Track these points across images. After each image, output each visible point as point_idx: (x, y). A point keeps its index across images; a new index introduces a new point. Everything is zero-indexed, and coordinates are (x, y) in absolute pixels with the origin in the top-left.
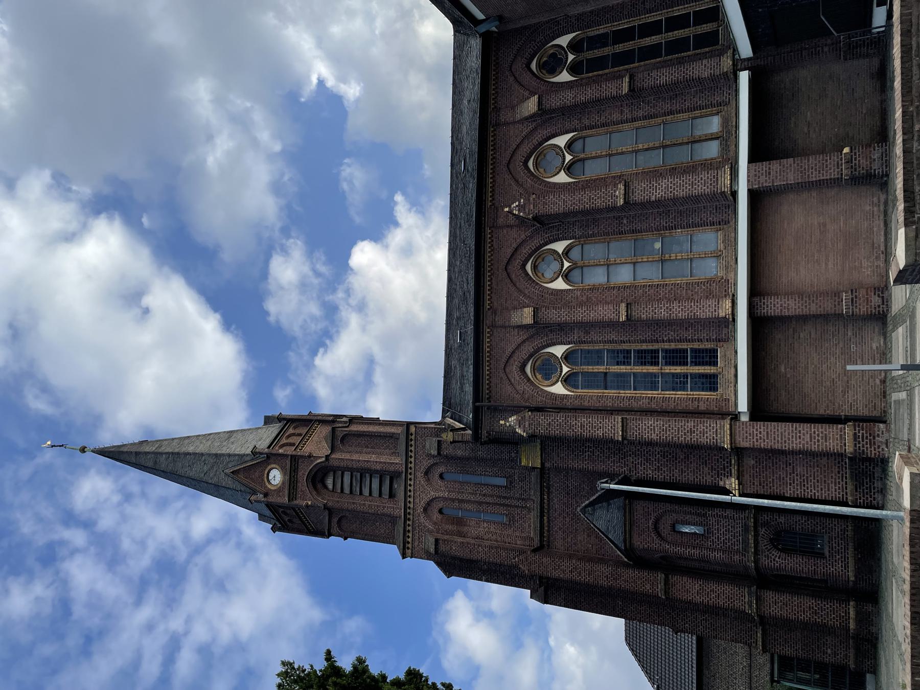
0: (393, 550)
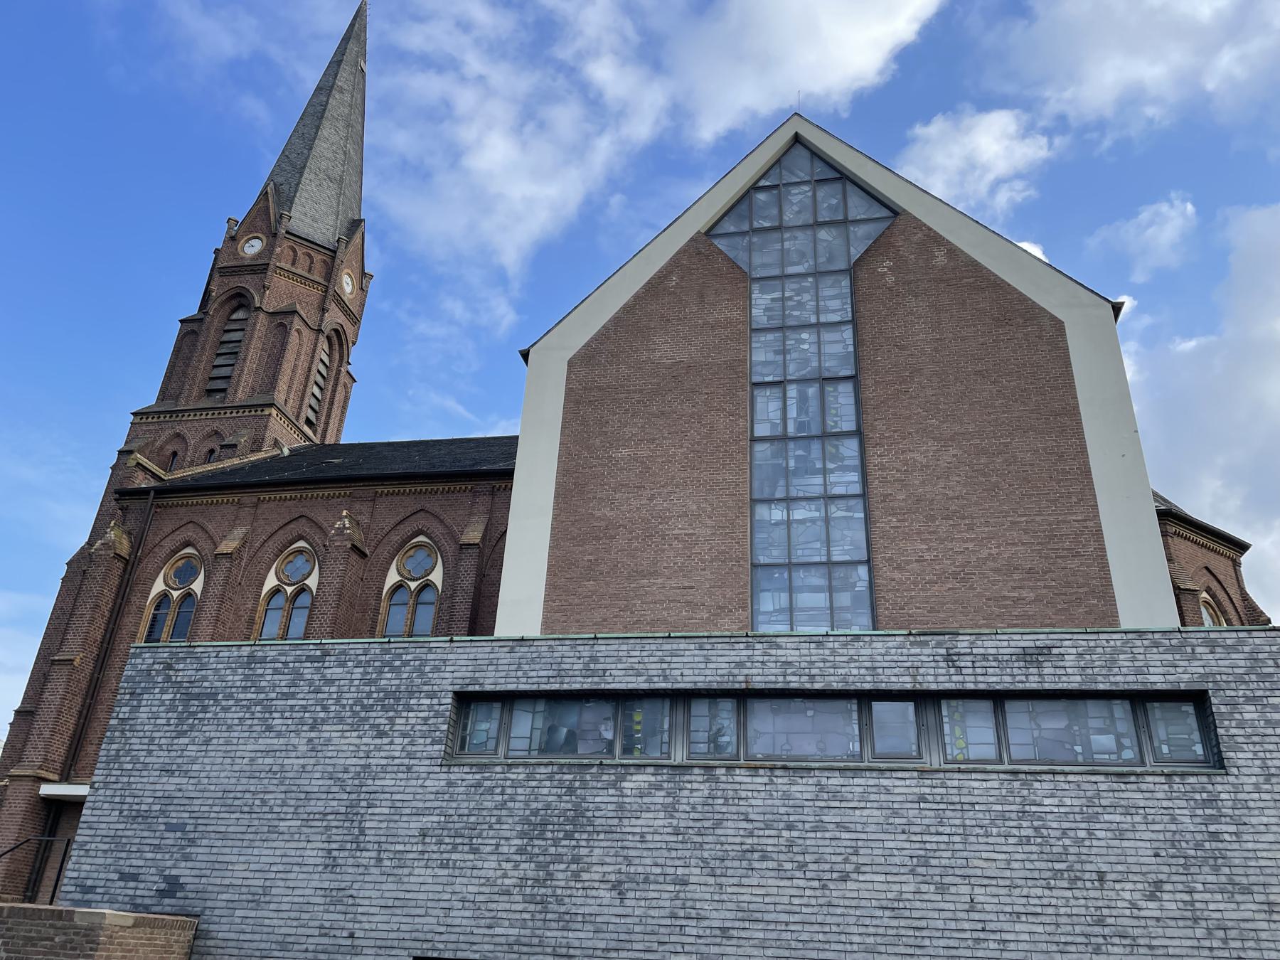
0: (149, 398)
